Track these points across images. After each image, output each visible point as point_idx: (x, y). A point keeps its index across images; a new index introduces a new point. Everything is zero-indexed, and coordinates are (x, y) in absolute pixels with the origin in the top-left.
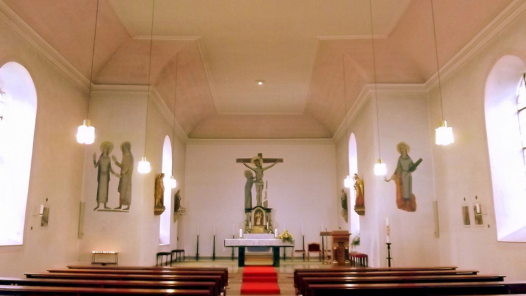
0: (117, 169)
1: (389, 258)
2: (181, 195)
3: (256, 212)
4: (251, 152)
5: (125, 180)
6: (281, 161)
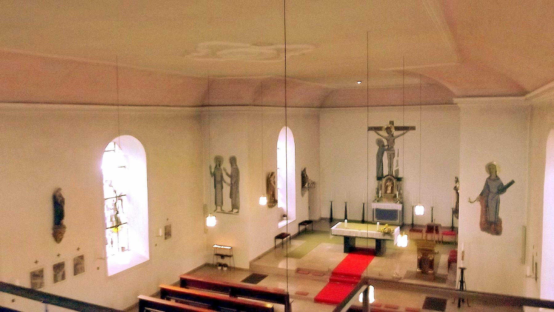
0: (227, 179)
4: (382, 118)
6: (413, 128)
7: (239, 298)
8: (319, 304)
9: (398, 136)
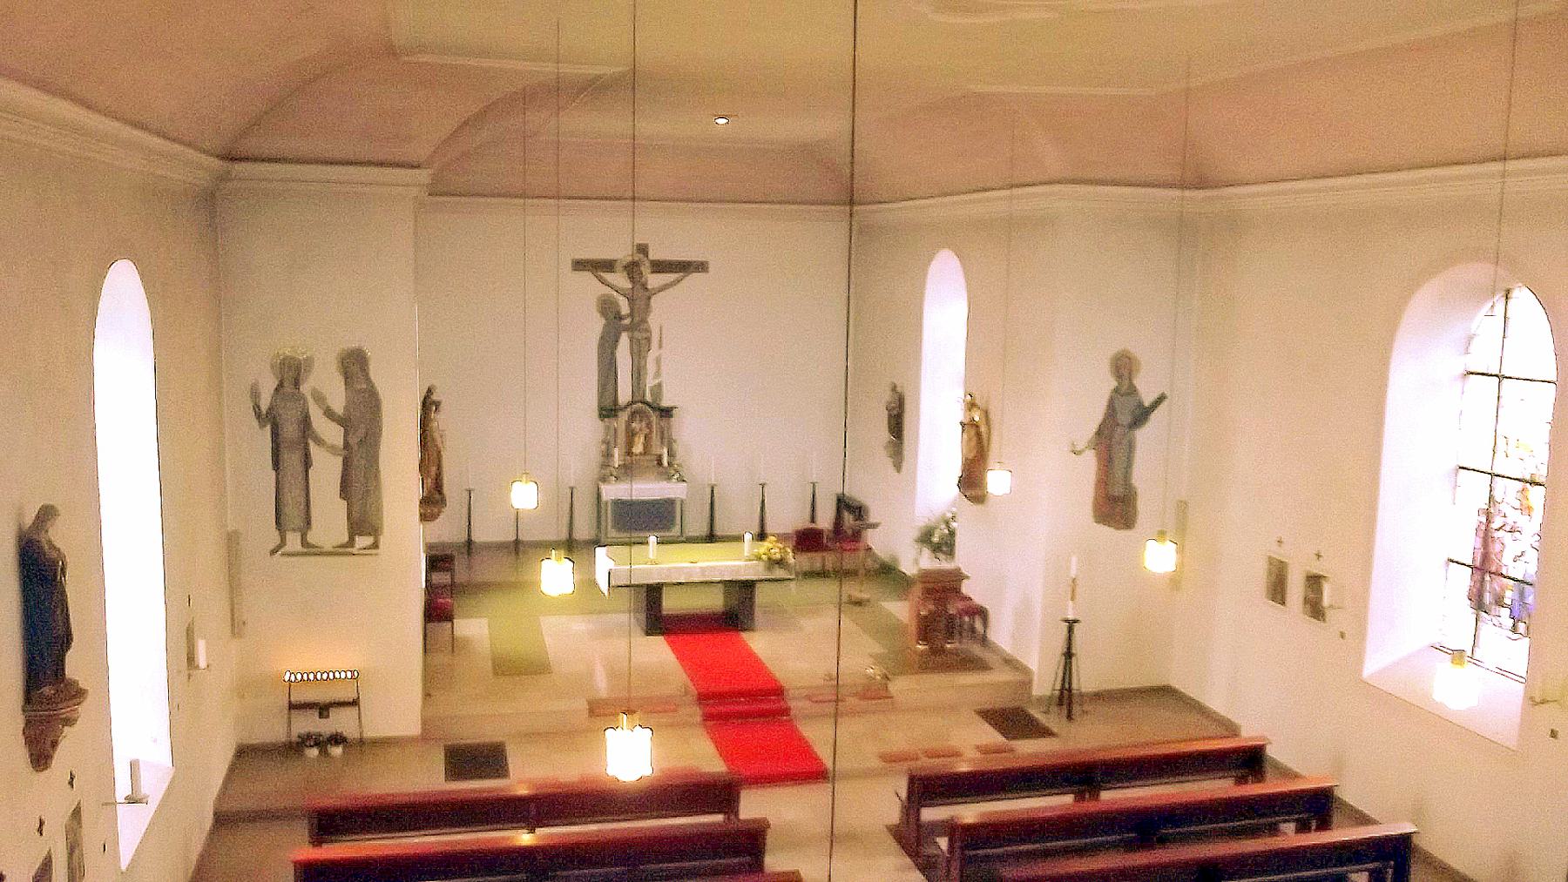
0: (332, 433)
1: (1069, 655)
3: (633, 414)
5: (359, 462)
6: (701, 267)
7: (1106, 795)
8: (814, 787)
9: (661, 289)
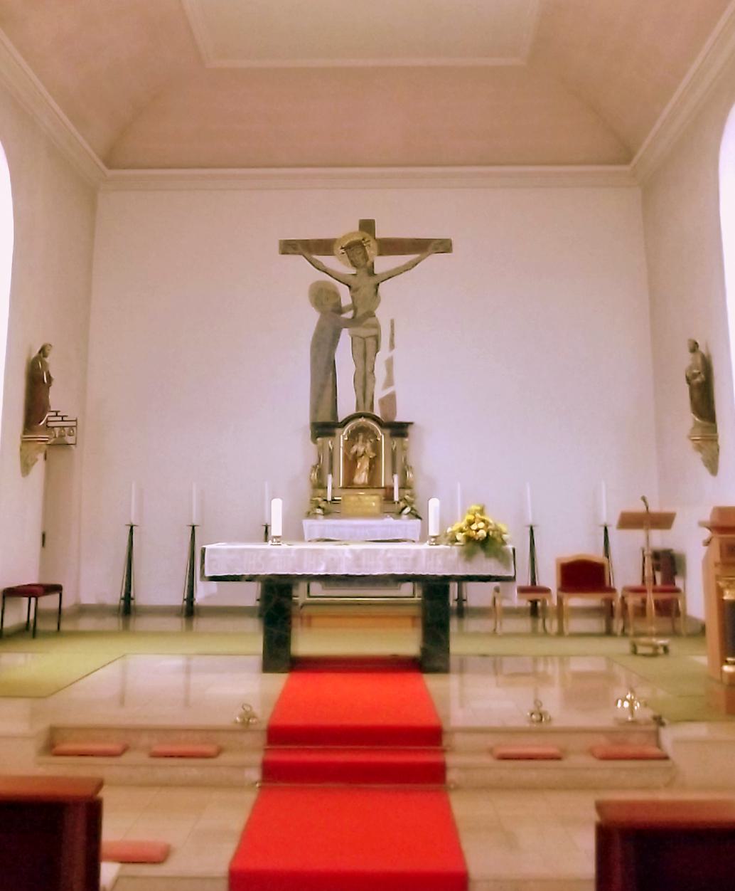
2: (54, 365)
3: (353, 436)
6: (444, 246)
